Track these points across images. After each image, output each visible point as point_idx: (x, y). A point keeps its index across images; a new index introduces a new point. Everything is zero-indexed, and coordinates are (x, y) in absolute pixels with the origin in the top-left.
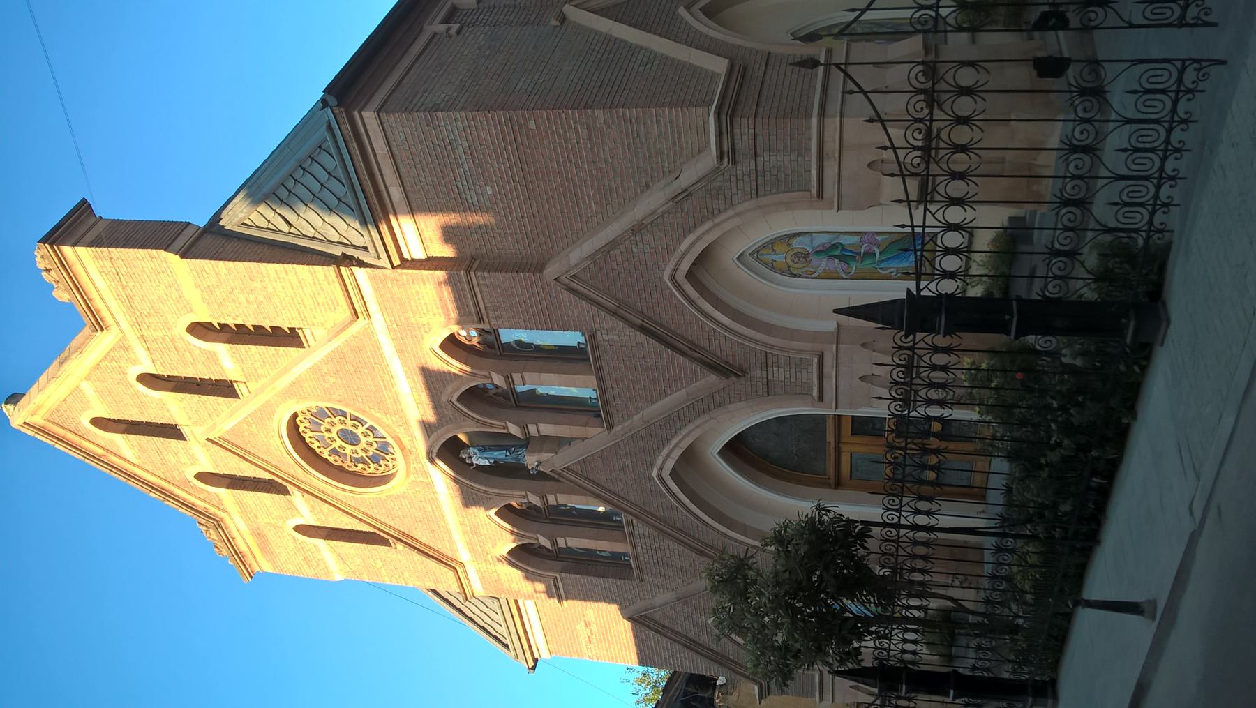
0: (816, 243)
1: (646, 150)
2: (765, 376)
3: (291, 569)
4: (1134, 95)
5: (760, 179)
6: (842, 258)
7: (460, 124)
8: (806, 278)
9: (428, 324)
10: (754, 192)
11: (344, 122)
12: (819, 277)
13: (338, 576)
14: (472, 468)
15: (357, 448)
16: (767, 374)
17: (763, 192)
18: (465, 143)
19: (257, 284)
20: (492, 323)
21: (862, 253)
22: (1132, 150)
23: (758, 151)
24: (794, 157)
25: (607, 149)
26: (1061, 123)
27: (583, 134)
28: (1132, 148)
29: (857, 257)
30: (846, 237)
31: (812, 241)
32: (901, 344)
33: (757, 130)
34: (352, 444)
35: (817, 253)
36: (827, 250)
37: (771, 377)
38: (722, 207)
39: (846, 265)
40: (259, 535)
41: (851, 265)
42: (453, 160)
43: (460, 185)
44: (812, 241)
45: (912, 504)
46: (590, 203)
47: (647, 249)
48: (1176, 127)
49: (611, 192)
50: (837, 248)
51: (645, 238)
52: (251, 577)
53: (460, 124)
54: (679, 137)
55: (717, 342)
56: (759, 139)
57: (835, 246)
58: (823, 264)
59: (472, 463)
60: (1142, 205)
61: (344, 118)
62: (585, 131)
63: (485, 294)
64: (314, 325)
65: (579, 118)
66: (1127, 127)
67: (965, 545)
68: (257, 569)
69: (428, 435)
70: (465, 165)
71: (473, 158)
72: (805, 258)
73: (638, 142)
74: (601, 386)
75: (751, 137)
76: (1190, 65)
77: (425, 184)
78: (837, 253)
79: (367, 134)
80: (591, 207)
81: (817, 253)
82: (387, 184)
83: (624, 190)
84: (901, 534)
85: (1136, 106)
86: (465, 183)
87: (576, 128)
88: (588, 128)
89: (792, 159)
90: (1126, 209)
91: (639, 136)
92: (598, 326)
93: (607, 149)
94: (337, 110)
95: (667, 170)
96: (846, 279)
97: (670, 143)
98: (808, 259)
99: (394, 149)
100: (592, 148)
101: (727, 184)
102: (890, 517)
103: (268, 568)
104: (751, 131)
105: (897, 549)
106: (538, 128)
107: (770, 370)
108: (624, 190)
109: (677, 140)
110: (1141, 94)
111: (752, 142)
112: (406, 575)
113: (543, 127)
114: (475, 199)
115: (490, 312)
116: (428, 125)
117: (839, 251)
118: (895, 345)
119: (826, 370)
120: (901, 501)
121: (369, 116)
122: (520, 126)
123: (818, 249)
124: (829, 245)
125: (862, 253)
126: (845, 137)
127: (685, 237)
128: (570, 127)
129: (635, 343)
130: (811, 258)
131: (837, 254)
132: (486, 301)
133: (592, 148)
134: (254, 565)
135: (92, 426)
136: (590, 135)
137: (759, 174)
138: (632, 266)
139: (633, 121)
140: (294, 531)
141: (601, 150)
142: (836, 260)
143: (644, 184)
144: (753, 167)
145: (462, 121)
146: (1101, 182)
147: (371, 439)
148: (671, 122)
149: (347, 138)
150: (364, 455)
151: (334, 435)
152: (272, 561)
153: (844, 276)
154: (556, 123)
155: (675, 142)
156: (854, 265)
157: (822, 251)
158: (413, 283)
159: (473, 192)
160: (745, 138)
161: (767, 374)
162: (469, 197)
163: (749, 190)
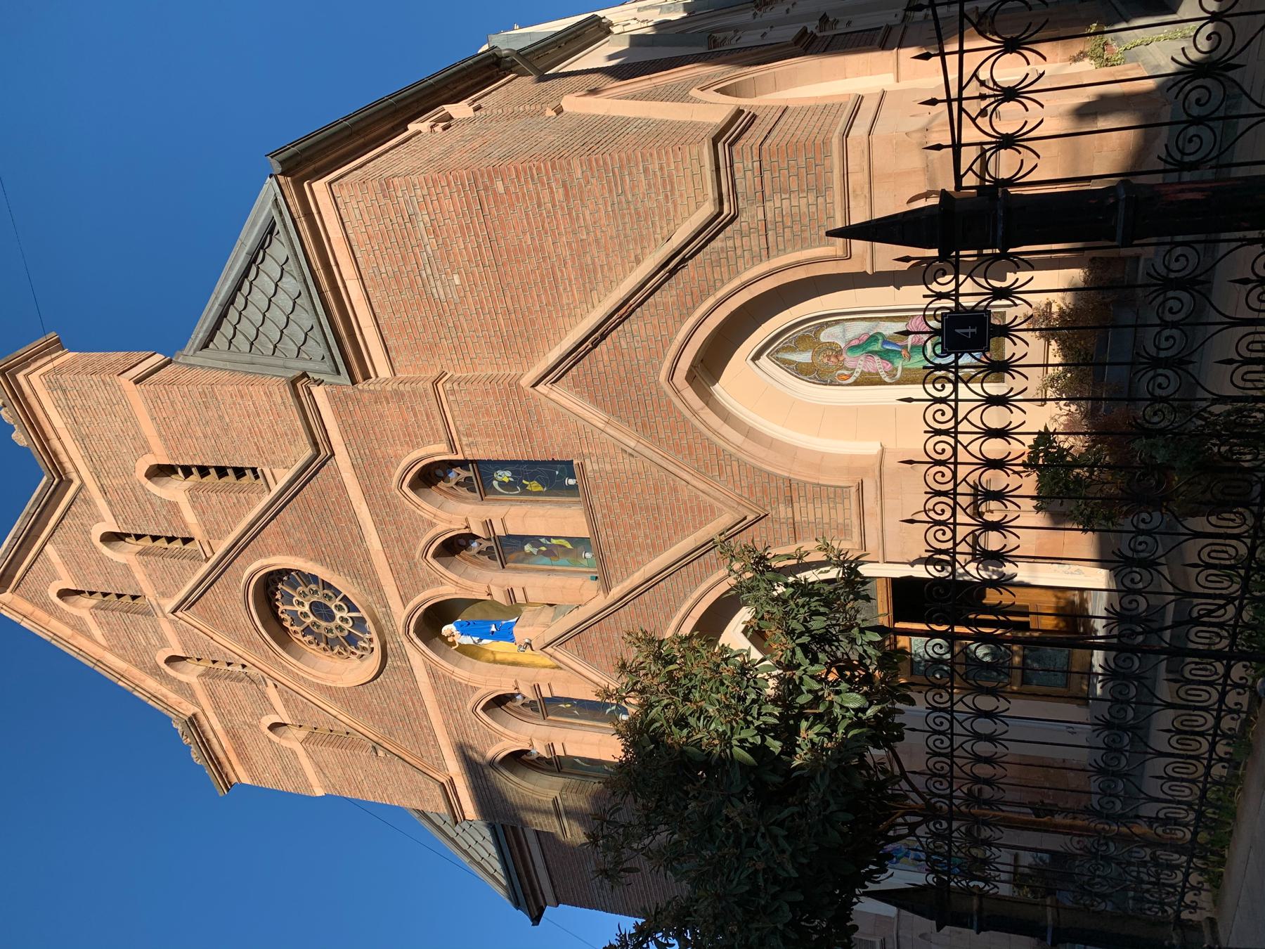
0: (850, 335)
1: (633, 212)
2: (790, 515)
3: (269, 782)
4: (1228, 366)
5: (770, 233)
6: (884, 355)
7: (419, 192)
8: (839, 385)
9: (396, 456)
10: (764, 253)
11: (291, 196)
12: (856, 383)
13: (319, 792)
14: (454, 648)
15: (332, 625)
16: (793, 513)
17: (775, 253)
18: (426, 218)
19: (212, 413)
20: (466, 453)
21: (909, 347)
22: (1257, 281)
23: (767, 193)
24: (812, 199)
25: (587, 213)
26: (1167, 127)
27: (559, 194)
28: (1240, 359)
29: (903, 353)
30: (888, 324)
31: (844, 331)
32: (938, 426)
33: (764, 163)
34: (327, 620)
35: (852, 348)
36: (863, 343)
37: (797, 518)
38: (726, 276)
39: (890, 365)
40: (233, 735)
41: (896, 365)
42: (414, 242)
43: (424, 275)
44: (844, 331)
45: (974, 417)
46: (572, 290)
47: (638, 342)
48: (1201, 776)
49: (595, 271)
50: (877, 340)
51: (634, 327)
52: (228, 790)
53: (419, 192)
54: (672, 190)
55: (729, 468)
56: (767, 175)
57: (873, 338)
58: (860, 364)
59: (454, 641)
60: (1202, 734)
61: (290, 191)
62: (561, 191)
63: (456, 413)
64: (274, 463)
65: (553, 172)
66: (1172, 711)
67: (1063, 766)
68: (234, 780)
69: (404, 605)
70: (428, 247)
71: (436, 236)
72: (836, 357)
73: (624, 200)
74: (592, 520)
75: (757, 173)
76: (1204, 754)
77: (385, 275)
78: (877, 347)
79: (319, 213)
80: (573, 295)
81: (852, 348)
82: (345, 278)
83: (610, 269)
84: (960, 477)
85: (1202, 549)
86: (429, 271)
87: (550, 188)
88: (565, 186)
89: (810, 203)
90: (1245, 368)
91: (624, 192)
92: (586, 451)
93: (587, 213)
94: (281, 178)
95: (659, 237)
96: (890, 384)
97: (661, 197)
98: (841, 359)
99: (349, 232)
100: (570, 214)
101: (730, 243)
102: (938, 721)
103: (246, 780)
104: (757, 164)
105: (955, 449)
106: (507, 189)
107: (796, 505)
108: (610, 269)
109: (669, 194)
110: (1237, 364)
111: (757, 180)
112: (390, 791)
113: (512, 189)
114: (442, 292)
115: (462, 437)
116: (384, 196)
117: (880, 345)
118: (929, 490)
119: (867, 505)
120: (955, 411)
121: (320, 186)
122: (486, 189)
123: (855, 343)
124: (866, 337)
125: (909, 347)
126: (875, 163)
127: (682, 323)
128: (543, 184)
129: (630, 473)
130: (844, 355)
131: (877, 349)
132: (458, 423)
133: (570, 214)
134: (232, 775)
135: (58, 599)
136: (567, 194)
137: (769, 226)
138: (622, 368)
139: (616, 170)
140: (268, 731)
141: (581, 215)
142: (876, 358)
143: (633, 258)
144: (761, 216)
145: (422, 188)
146: (1243, 124)
147: (345, 614)
148: (661, 169)
149: (295, 216)
150: (339, 634)
151: (306, 609)
152: (249, 770)
153: (887, 380)
154: (526, 182)
155: (667, 196)
156: (899, 364)
157: (857, 347)
158: (376, 402)
159: (439, 283)
160: (749, 174)
161: (793, 513)
162: (434, 290)
163: (758, 249)
